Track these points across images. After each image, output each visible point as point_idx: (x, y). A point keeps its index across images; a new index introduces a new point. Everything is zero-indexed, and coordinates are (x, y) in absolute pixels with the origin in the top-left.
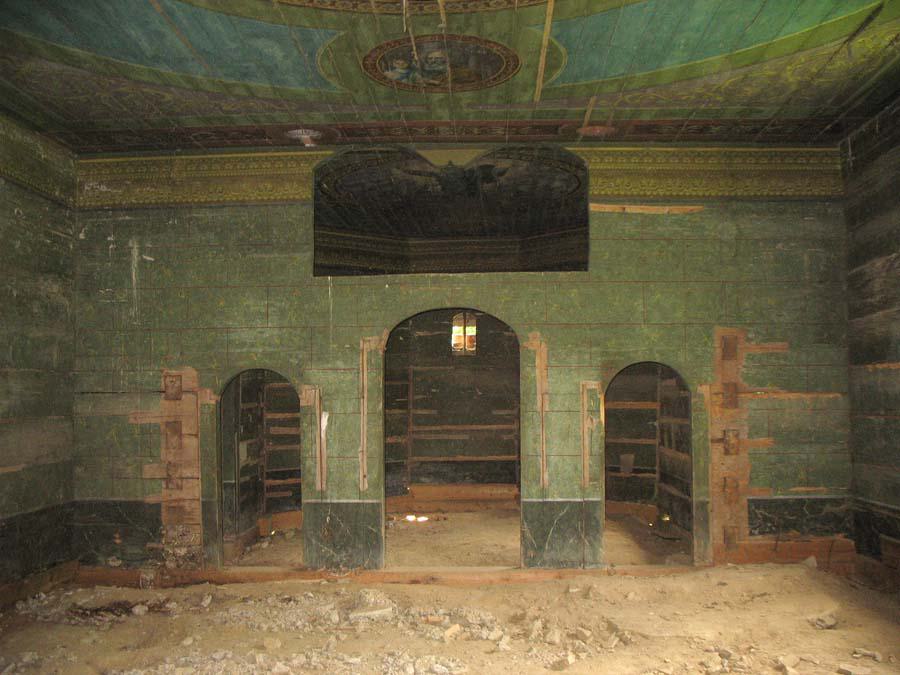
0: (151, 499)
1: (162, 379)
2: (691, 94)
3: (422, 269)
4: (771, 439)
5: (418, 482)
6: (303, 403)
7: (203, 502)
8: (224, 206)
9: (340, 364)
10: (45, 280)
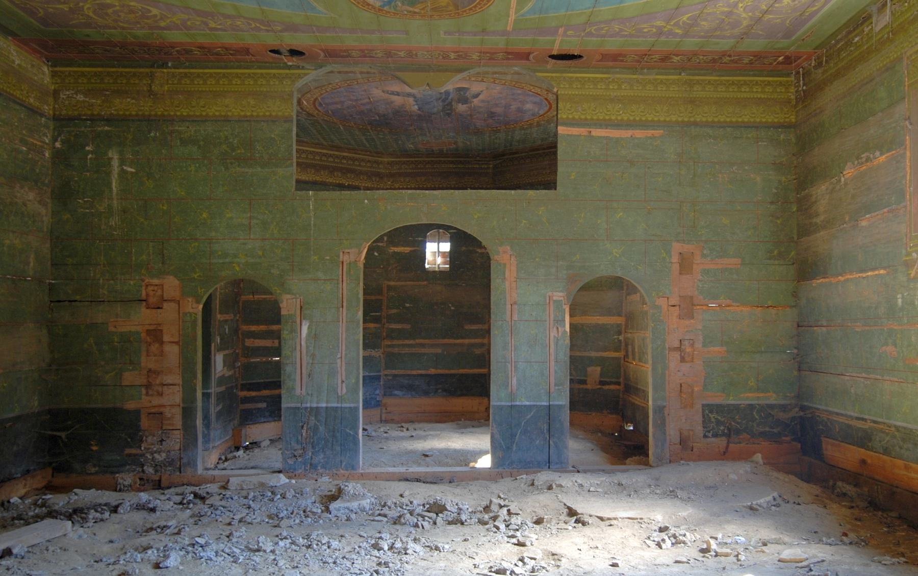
0: (131, 405)
1: (144, 288)
2: (652, 26)
3: (488, 186)
4: (725, 348)
5: (391, 395)
6: (284, 312)
7: (183, 408)
8: (206, 121)
9: (320, 275)
10: (22, 187)
